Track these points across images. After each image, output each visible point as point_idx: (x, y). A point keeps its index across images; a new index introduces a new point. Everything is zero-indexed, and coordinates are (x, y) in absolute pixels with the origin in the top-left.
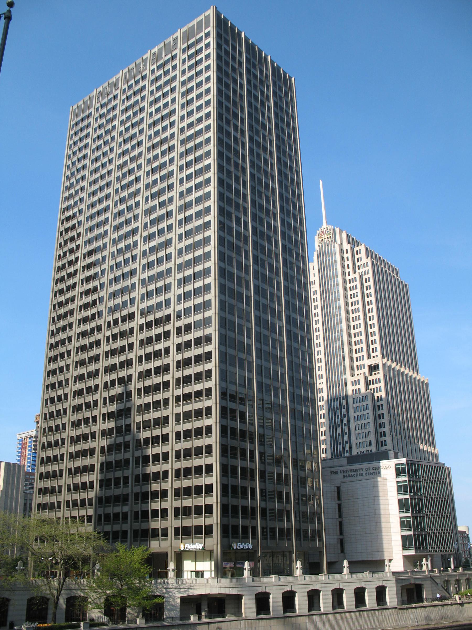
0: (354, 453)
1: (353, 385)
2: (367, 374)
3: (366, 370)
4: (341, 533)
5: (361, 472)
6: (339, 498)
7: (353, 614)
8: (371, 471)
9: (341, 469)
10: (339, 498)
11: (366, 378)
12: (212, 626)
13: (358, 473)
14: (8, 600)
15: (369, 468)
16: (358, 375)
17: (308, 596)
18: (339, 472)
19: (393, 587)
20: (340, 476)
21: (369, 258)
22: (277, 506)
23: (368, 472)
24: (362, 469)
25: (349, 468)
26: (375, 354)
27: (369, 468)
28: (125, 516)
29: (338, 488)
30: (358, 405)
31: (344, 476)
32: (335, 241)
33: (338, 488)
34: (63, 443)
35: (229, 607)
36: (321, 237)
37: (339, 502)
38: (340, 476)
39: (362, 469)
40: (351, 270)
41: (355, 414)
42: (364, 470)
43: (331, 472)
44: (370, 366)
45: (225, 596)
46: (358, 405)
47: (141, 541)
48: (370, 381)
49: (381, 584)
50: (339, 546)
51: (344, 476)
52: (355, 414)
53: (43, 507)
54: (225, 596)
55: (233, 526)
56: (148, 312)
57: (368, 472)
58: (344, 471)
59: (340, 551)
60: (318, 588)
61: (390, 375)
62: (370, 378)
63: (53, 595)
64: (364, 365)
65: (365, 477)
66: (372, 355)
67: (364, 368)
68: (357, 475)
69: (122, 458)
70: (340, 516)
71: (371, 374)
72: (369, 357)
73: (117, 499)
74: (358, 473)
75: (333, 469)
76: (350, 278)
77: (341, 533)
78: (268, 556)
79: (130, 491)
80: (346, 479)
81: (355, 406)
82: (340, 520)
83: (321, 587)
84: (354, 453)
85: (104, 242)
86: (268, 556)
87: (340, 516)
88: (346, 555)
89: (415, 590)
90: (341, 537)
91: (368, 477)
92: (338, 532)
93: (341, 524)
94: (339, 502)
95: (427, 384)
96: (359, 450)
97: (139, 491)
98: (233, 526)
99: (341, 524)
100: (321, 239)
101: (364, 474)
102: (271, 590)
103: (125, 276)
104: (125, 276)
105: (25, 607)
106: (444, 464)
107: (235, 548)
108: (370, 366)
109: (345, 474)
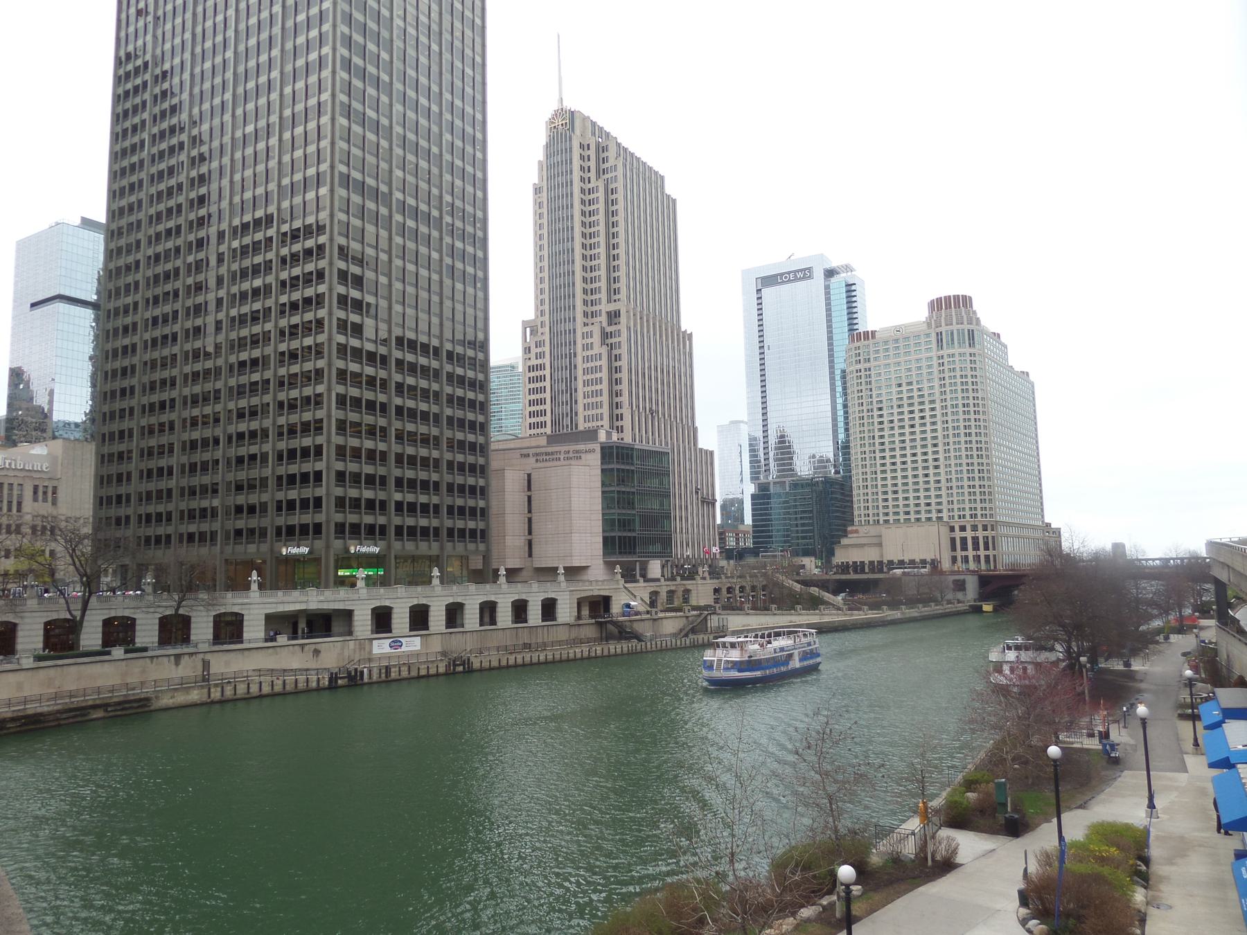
0: (581, 428)
2: (605, 324)
3: (604, 319)
4: (530, 533)
6: (529, 488)
7: (508, 631)
8: (571, 455)
10: (529, 488)
11: (603, 329)
14: (15, 625)
19: (24, 637)
20: (532, 460)
25: (550, 450)
26: (617, 297)
28: (264, 507)
29: (529, 475)
31: (537, 461)
32: (573, 130)
33: (529, 475)
34: (172, 407)
35: (336, 627)
37: (529, 493)
38: (532, 460)
40: (593, 175)
41: (585, 378)
44: (609, 314)
45: (601, 599)
47: (286, 540)
49: (120, 613)
52: (585, 378)
54: (601, 599)
58: (537, 455)
59: (527, 555)
60: (524, 597)
61: (635, 325)
62: (609, 329)
63: (74, 617)
65: (562, 462)
66: (614, 297)
69: (311, 419)
70: (530, 511)
72: (609, 301)
73: (204, 489)
75: (525, 452)
76: (590, 186)
77: (530, 533)
79: (270, 472)
80: (539, 465)
82: (529, 515)
84: (581, 428)
85: (170, 164)
87: (530, 511)
90: (529, 537)
91: (566, 462)
93: (530, 520)
94: (529, 493)
95: (690, 335)
96: (587, 425)
97: (283, 473)
99: (530, 520)
105: (42, 632)
108: (609, 314)
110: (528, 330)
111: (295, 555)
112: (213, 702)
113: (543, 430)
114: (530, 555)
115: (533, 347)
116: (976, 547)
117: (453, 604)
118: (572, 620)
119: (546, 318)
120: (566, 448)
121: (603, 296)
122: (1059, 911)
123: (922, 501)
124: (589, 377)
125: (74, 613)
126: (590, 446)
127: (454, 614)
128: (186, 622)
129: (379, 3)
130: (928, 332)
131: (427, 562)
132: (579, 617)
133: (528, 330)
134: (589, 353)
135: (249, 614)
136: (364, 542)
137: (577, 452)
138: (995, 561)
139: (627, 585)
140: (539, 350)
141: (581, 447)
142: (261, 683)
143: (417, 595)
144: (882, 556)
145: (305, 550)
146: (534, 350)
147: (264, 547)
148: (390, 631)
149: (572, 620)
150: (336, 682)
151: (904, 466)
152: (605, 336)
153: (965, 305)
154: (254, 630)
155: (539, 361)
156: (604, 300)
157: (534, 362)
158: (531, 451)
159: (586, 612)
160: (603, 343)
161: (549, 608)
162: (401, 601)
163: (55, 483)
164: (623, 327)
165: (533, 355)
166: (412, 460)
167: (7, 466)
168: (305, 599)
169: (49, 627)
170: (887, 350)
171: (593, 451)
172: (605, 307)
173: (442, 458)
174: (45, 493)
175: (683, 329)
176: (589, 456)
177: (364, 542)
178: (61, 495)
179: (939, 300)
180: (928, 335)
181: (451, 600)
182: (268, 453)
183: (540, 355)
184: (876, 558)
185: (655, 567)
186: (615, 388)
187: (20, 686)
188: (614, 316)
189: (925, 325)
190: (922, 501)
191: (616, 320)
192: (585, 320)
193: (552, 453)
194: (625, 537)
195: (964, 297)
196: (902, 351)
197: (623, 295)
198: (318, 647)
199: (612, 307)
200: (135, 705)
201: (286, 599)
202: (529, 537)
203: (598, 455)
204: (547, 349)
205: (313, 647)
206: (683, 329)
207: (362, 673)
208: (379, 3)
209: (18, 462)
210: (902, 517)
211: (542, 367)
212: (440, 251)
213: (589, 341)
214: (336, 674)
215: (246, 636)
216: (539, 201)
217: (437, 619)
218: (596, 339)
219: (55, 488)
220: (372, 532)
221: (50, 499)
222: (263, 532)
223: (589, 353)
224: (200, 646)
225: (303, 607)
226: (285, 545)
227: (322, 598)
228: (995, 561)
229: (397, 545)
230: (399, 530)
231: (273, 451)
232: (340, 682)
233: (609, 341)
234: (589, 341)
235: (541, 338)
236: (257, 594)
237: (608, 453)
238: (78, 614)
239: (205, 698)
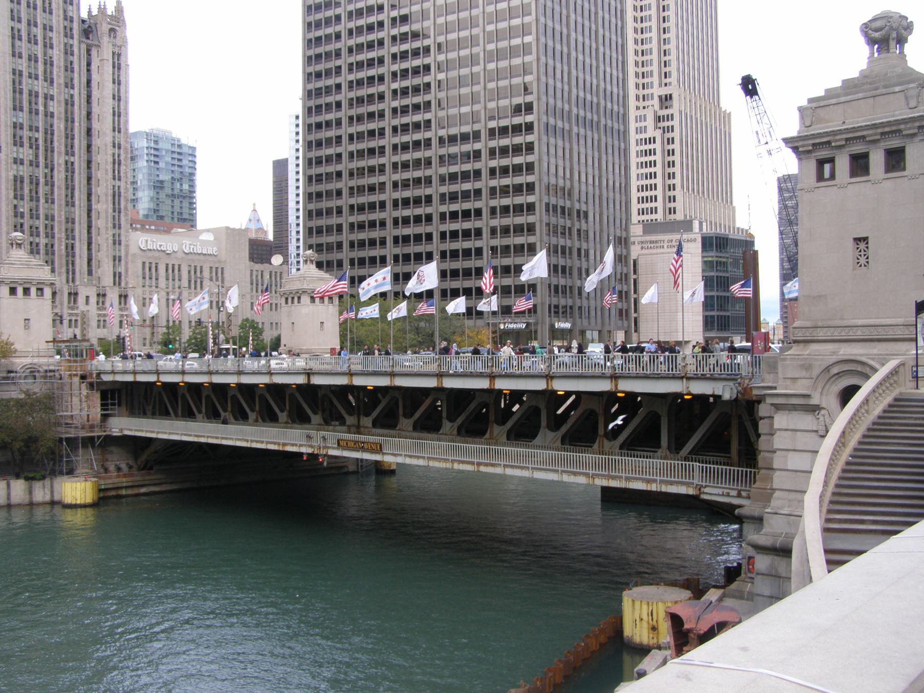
2: (657, 107)
3: (656, 102)
5: (662, 244)
9: (640, 239)
11: (655, 112)
13: (659, 245)
15: (672, 241)
16: (644, 108)
18: (636, 243)
21: (34, 202)
22: (577, 263)
23: (670, 244)
24: (664, 241)
26: (668, 80)
27: (672, 241)
31: (642, 248)
39: (664, 241)
42: (666, 242)
44: (660, 97)
45: (539, 281)
48: (659, 117)
51: (642, 248)
53: (70, 321)
55: (561, 246)
56: (326, 6)
57: (670, 244)
58: (642, 242)
64: (652, 94)
67: (652, 99)
68: (657, 247)
71: (661, 108)
72: (660, 85)
74: (659, 245)
80: (644, 251)
95: (730, 114)
98: (561, 246)
101: (665, 247)
106: (801, 109)
113: (654, 217)
121: (655, 79)
122: (788, 269)
126: (691, 236)
129: (553, 2)
136: (561, 319)
152: (658, 119)
156: (656, 84)
160: (656, 128)
164: (674, 110)
167: (192, 251)
171: (695, 240)
172: (657, 91)
175: (723, 110)
176: (691, 245)
177: (561, 319)
186: (663, 36)
188: (666, 100)
191: (668, 103)
192: (637, 103)
193: (656, 242)
194: (721, 316)
197: (673, 79)
199: (664, 91)
201: (18, 253)
203: (698, 245)
206: (723, 110)
208: (553, 2)
209: (198, 247)
212: (570, 122)
213: (643, 124)
218: (650, 122)
223: (643, 136)
233: (661, 124)
234: (643, 124)
237: (709, 243)
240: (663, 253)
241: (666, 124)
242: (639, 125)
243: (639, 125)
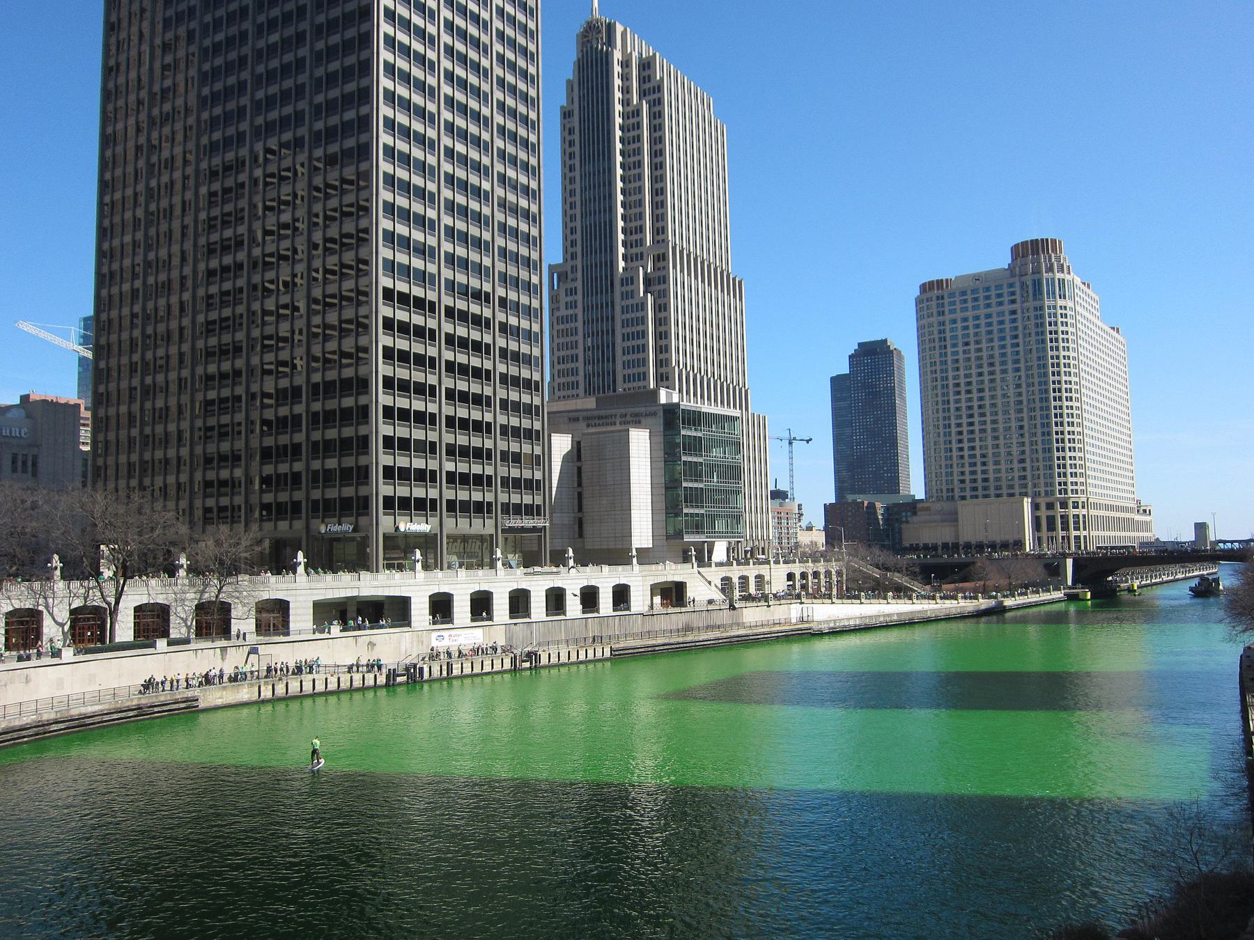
1: (622, 285)
12: (360, 639)
15: (626, 415)
17: (471, 600)
25: (602, 413)
27: (626, 415)
30: (628, 316)
36: (586, 37)
37: (579, 464)
39: (615, 416)
43: (570, 419)
46: (628, 316)
50: (576, 527)
51: (588, 426)
58: (588, 418)
59: (577, 535)
63: (109, 604)
68: (607, 424)
77: (580, 509)
78: (459, 541)
80: (592, 430)
81: (624, 317)
83: (287, 596)
86: (459, 541)
88: (961, 542)
89: (674, 590)
90: (580, 515)
92: (576, 509)
94: (579, 464)
100: (585, 40)
102: (287, 596)
103: (228, 93)
104: (228, 93)
107: (323, 532)
109: (590, 422)
110: (555, 275)
111: (337, 532)
112: (263, 702)
114: (581, 535)
115: (562, 294)
116: (1065, 527)
117: (588, 587)
118: (645, 609)
119: (579, 262)
120: (623, 411)
123: (979, 477)
124: (629, 330)
125: (108, 599)
127: (519, 602)
128: (225, 609)
130: (1011, 280)
131: (479, 543)
132: (652, 607)
133: (555, 275)
134: (630, 302)
135: (296, 601)
137: (637, 415)
138: (1085, 542)
139: (701, 570)
140: (569, 299)
141: (642, 410)
142: (314, 680)
143: (479, 580)
144: (957, 536)
145: (347, 527)
146: (563, 299)
147: (299, 525)
148: (288, 634)
149: (645, 609)
150: (394, 680)
151: (971, 436)
153: (1054, 250)
154: (301, 618)
155: (570, 312)
157: (563, 312)
158: (582, 414)
159: (657, 600)
161: (621, 595)
162: (538, 585)
163: (35, 451)
165: (562, 306)
166: (464, 424)
168: (357, 583)
169: (201, 608)
170: (976, 299)
173: (495, 422)
174: (24, 463)
178: (42, 464)
179: (1024, 244)
180: (1011, 285)
181: (436, 590)
182: (300, 415)
183: (573, 305)
184: (949, 539)
185: (720, 551)
187: (60, 683)
189: (1009, 272)
190: (979, 477)
193: (606, 417)
195: (1054, 241)
196: (970, 305)
198: (373, 639)
200: (183, 705)
201: (336, 584)
202: (580, 515)
204: (579, 297)
205: (367, 639)
207: (421, 669)
210: (980, 492)
211: (574, 318)
214: (394, 670)
215: (293, 626)
216: (568, 126)
217: (501, 606)
219: (35, 458)
220: (422, 506)
221: (30, 469)
222: (296, 507)
223: (630, 302)
224: (1182, 591)
225: (355, 593)
226: (323, 522)
227: (376, 583)
228: (1085, 542)
229: (449, 523)
230: (451, 505)
231: (307, 412)
232: (399, 679)
235: (573, 285)
236: (305, 577)
238: (112, 600)
239: (255, 697)
240: (612, 432)
241: (652, 97)
242: (625, 289)
243: (625, 289)
